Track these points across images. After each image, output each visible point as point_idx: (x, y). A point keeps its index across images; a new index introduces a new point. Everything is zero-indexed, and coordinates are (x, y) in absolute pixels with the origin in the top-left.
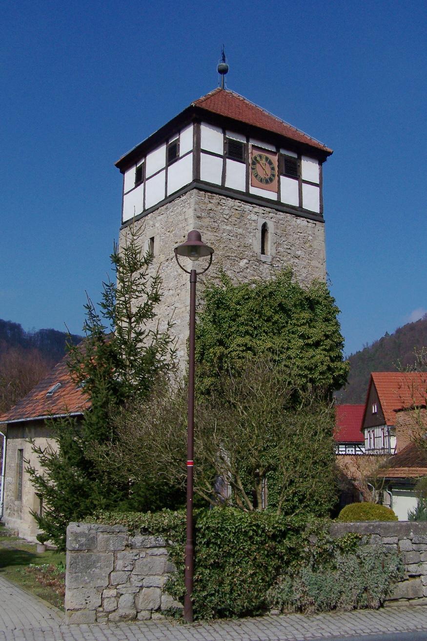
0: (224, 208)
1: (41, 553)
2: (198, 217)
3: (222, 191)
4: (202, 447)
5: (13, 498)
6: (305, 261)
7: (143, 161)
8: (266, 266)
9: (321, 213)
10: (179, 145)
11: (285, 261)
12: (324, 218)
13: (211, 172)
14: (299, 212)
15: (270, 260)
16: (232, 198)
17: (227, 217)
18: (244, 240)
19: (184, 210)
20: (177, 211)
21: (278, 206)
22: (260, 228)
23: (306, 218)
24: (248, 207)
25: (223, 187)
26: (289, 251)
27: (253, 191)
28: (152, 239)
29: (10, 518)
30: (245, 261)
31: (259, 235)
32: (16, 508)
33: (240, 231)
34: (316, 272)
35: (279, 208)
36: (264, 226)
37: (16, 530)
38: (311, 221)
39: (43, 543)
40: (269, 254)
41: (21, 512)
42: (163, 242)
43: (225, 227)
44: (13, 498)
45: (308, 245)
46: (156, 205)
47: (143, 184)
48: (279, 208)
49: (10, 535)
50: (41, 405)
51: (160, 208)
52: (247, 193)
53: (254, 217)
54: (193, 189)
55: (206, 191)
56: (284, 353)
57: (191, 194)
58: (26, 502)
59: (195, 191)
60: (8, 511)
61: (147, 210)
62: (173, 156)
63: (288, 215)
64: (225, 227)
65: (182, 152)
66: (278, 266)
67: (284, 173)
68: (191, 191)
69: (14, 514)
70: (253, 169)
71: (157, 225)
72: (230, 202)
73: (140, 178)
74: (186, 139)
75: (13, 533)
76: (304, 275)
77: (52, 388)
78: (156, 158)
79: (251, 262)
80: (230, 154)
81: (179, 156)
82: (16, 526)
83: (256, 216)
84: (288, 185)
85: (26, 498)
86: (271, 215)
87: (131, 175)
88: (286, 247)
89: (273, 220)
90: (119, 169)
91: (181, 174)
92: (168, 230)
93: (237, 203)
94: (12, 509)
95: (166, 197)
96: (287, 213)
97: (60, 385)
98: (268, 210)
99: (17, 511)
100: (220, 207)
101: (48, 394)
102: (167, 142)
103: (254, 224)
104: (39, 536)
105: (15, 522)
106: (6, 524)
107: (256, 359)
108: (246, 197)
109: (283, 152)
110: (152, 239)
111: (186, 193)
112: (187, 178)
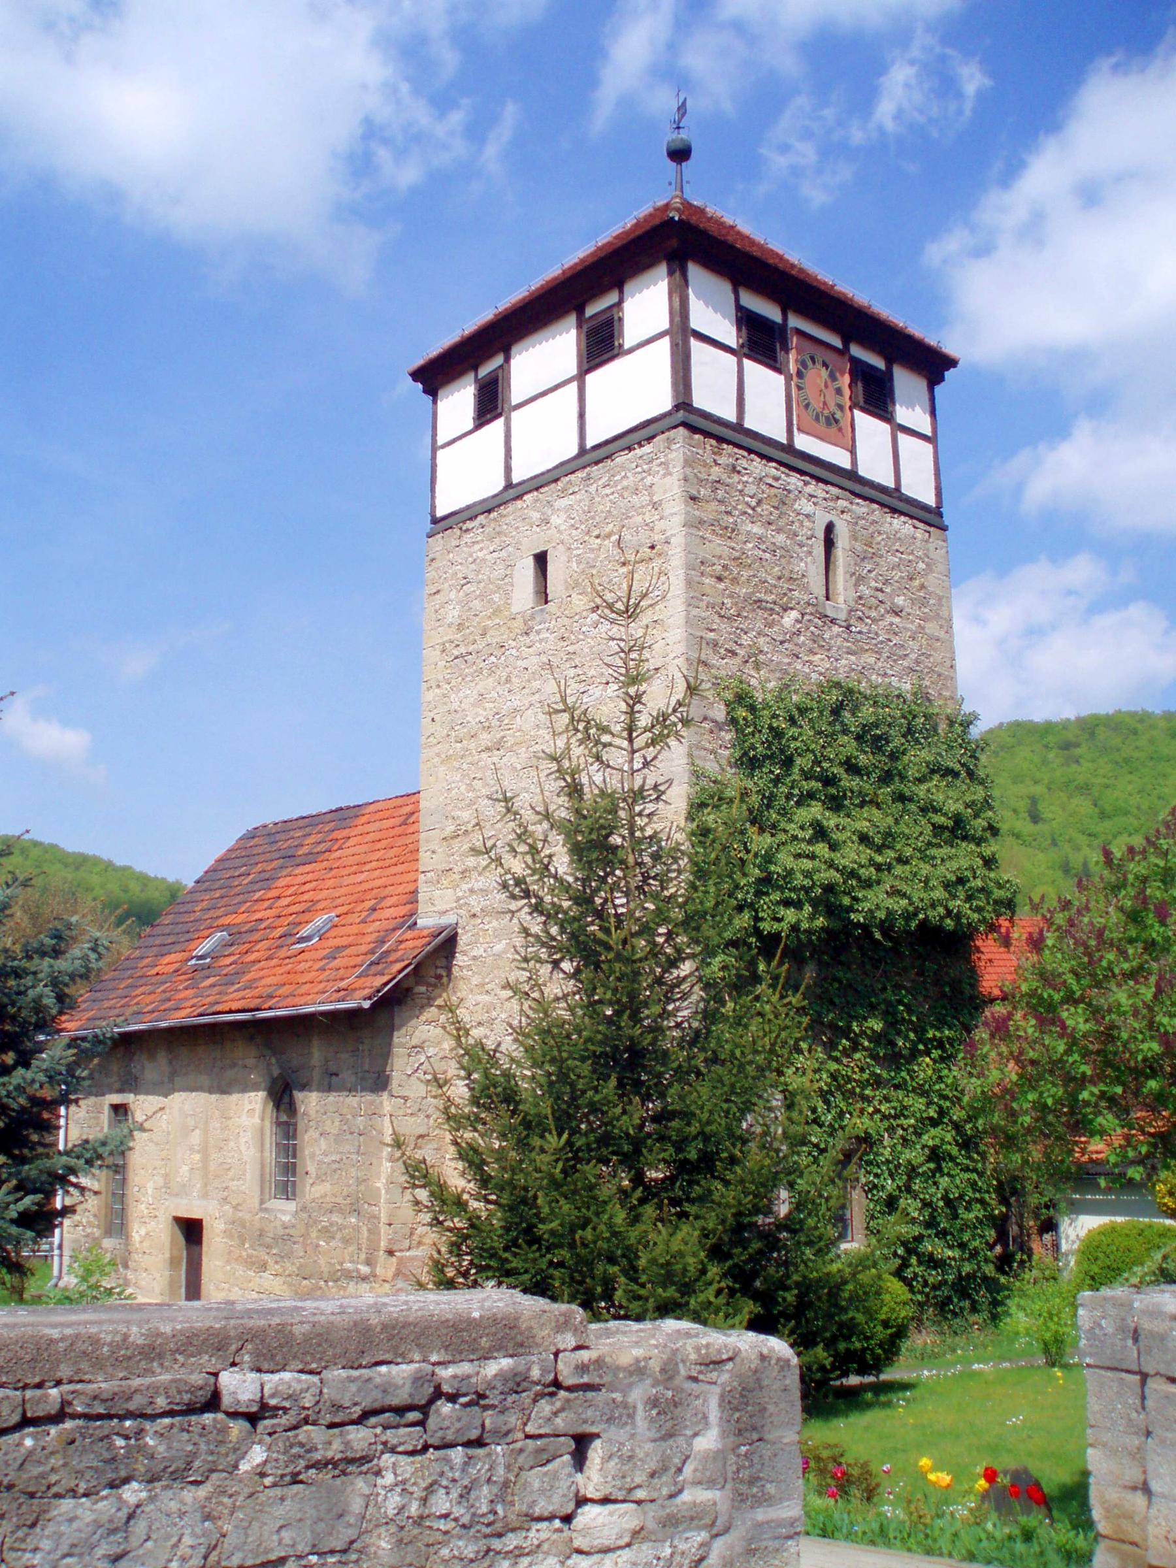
0: (745, 479)
2: (693, 498)
3: (730, 435)
5: (97, 1232)
6: (912, 622)
7: (499, 360)
8: (836, 629)
9: (938, 507)
10: (621, 320)
11: (874, 620)
12: (947, 520)
13: (716, 382)
14: (892, 500)
15: (842, 616)
16: (762, 456)
17: (753, 504)
18: (789, 563)
19: (649, 480)
20: (625, 483)
21: (851, 482)
22: (821, 535)
23: (912, 517)
24: (795, 480)
25: (739, 427)
26: (880, 596)
27: (803, 443)
28: (541, 560)
30: (794, 614)
31: (819, 550)
33: (781, 539)
34: (935, 650)
35: (858, 488)
36: (830, 528)
38: (921, 525)
40: (841, 599)
41: (126, 1266)
42: (579, 563)
43: (749, 527)
45: (917, 583)
46: (549, 471)
47: (500, 422)
48: (858, 488)
51: (565, 480)
52: (789, 448)
53: (806, 507)
54: (675, 427)
55: (707, 434)
57: (670, 441)
59: (681, 430)
61: (520, 484)
62: (601, 345)
63: (876, 506)
64: (749, 527)
65: (631, 334)
66: (860, 632)
67: (862, 403)
68: (672, 433)
70: (799, 388)
71: (555, 520)
72: (757, 466)
73: (491, 404)
74: (645, 306)
76: (913, 656)
77: (205, 947)
78: (550, 354)
79: (807, 617)
80: (750, 349)
81: (621, 346)
83: (814, 505)
84: (869, 429)
85: (143, 1232)
86: (842, 503)
87: (459, 401)
88: (873, 584)
89: (850, 516)
90: (420, 386)
91: (635, 387)
92: (596, 533)
93: (772, 469)
95: (583, 451)
96: (872, 501)
98: (835, 491)
100: (736, 478)
102: (580, 310)
103: (807, 523)
107: (836, 857)
108: (786, 456)
109: (856, 351)
110: (541, 560)
111: (653, 437)
112: (658, 399)
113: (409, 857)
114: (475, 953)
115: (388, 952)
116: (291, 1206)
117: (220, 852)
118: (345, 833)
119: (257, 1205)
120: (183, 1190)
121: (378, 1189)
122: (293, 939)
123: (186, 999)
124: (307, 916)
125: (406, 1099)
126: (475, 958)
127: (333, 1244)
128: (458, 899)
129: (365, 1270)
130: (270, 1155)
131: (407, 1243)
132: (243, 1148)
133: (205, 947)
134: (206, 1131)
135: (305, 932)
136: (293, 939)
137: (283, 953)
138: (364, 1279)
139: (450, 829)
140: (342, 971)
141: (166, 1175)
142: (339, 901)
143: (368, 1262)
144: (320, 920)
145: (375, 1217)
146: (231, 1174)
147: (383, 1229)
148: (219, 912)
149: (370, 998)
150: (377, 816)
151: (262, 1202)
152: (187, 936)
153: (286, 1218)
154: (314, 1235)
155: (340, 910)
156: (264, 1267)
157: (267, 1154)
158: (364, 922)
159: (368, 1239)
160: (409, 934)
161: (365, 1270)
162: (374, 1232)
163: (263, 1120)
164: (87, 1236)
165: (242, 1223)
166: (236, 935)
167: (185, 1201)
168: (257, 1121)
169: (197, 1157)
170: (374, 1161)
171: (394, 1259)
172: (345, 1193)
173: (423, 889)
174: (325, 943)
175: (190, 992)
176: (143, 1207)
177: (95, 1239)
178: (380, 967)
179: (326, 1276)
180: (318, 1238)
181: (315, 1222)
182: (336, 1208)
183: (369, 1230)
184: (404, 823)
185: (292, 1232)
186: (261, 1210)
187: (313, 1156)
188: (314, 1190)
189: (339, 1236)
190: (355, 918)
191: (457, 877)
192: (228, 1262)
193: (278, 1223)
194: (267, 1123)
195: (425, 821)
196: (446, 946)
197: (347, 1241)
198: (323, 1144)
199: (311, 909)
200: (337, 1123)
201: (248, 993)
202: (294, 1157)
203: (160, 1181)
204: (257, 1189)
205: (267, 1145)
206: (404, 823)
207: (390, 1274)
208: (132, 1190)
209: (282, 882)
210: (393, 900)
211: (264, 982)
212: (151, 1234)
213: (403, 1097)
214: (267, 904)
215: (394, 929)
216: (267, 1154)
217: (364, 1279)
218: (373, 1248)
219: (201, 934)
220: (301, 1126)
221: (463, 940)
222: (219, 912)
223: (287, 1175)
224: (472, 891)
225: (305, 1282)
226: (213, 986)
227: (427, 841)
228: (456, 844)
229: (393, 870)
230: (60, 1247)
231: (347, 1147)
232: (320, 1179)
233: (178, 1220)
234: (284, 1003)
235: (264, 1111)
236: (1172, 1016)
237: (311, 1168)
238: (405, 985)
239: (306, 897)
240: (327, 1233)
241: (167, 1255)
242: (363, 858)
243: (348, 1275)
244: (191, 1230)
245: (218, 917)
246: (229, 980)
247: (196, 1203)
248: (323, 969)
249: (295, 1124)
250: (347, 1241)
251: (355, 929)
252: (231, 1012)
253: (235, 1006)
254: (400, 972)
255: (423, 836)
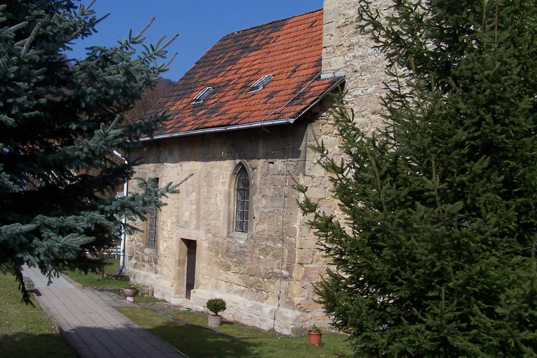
1: (215, 328)
4: (96, 215)
5: (142, 245)
29: (136, 271)
32: (146, 258)
37: (150, 288)
39: (216, 313)
41: (156, 263)
44: (141, 243)
49: (143, 294)
50: (257, 88)
56: (418, 75)
58: (164, 251)
60: (134, 261)
69: (144, 266)
75: (146, 291)
77: (199, 94)
82: (148, 282)
85: (165, 246)
94: (140, 259)
97: (212, 89)
99: (149, 262)
101: (194, 103)
104: (212, 304)
105: (146, 276)
106: (132, 279)
113: (317, 42)
114: (355, 93)
115: (304, 93)
116: (245, 236)
117: (209, 48)
118: (277, 34)
119: (226, 234)
120: (186, 225)
121: (295, 228)
122: (248, 89)
123: (189, 122)
124: (256, 77)
125: (313, 177)
126: (355, 96)
127: (268, 258)
128: (347, 62)
129: (285, 273)
130: (233, 207)
131: (310, 260)
132: (219, 203)
133: (199, 94)
134: (199, 193)
135: (254, 84)
136: (248, 89)
137: (243, 96)
138: (285, 278)
139: (342, 21)
140: (277, 104)
141: (177, 216)
142: (274, 68)
143: (288, 269)
144: (264, 78)
145: (292, 244)
146: (212, 217)
147: (297, 251)
148: (208, 78)
149: (294, 118)
150: (296, 24)
151: (228, 233)
152: (191, 90)
153: (242, 242)
154: (257, 251)
155: (274, 73)
156: (228, 268)
157: (232, 206)
158: (289, 77)
159: (288, 256)
160: (316, 83)
161: (285, 273)
162: (292, 252)
163: (230, 187)
164: (137, 246)
165: (218, 244)
166: (217, 89)
167: (187, 231)
168: (227, 188)
169: (194, 207)
170: (293, 212)
171: (303, 269)
172: (276, 230)
173: (324, 56)
174: (266, 90)
175: (192, 118)
176: (165, 233)
177: (141, 248)
178: (299, 101)
179: (263, 275)
180: (259, 254)
181: (258, 245)
182: (270, 238)
183: (289, 251)
184: (311, 26)
185: (245, 250)
186: (228, 237)
187: (258, 208)
188: (258, 227)
189: (271, 253)
190: (284, 76)
191: (346, 49)
192: (209, 264)
193: (237, 245)
194: (232, 190)
195: (326, 18)
196: (338, 87)
197: (275, 257)
198: (264, 202)
199: (258, 72)
200: (272, 190)
201: (223, 117)
202: (247, 209)
203: (174, 219)
204: (226, 225)
205: (232, 202)
206: (311, 26)
207: (300, 277)
208: (160, 224)
209: (241, 61)
210: (306, 66)
211: (232, 111)
212: (169, 246)
213: (311, 176)
214: (234, 72)
215: (307, 81)
216: (232, 206)
217: (285, 278)
218: (291, 261)
219: (199, 89)
220: (251, 192)
221: (349, 85)
222: (208, 78)
223: (243, 219)
224: (354, 57)
225: (251, 278)
226: (204, 114)
227: (328, 29)
228: (345, 29)
229: (305, 50)
230: (124, 251)
231: (277, 204)
232: (261, 221)
233: (183, 240)
234: (244, 121)
235: (230, 183)
236: (533, 330)
237: (256, 215)
238: (314, 111)
239: (255, 67)
240: (265, 251)
241: (177, 259)
242: (287, 46)
243: (276, 276)
244: (191, 245)
245: (207, 80)
246: (213, 111)
247: (193, 232)
248: (266, 103)
249: (248, 191)
250: (275, 257)
251: (283, 82)
252: (213, 127)
253: (215, 124)
254: (312, 103)
255: (325, 27)
